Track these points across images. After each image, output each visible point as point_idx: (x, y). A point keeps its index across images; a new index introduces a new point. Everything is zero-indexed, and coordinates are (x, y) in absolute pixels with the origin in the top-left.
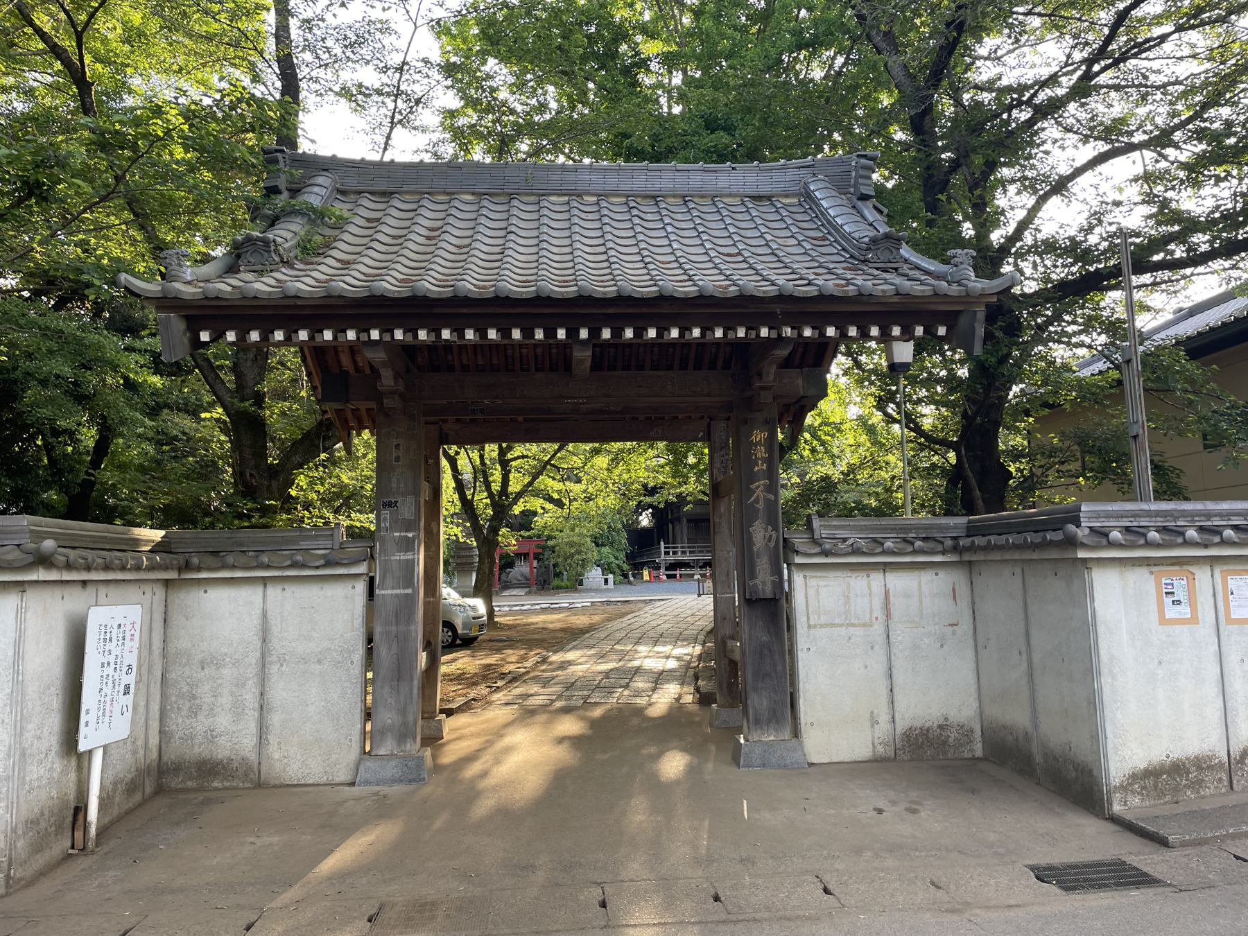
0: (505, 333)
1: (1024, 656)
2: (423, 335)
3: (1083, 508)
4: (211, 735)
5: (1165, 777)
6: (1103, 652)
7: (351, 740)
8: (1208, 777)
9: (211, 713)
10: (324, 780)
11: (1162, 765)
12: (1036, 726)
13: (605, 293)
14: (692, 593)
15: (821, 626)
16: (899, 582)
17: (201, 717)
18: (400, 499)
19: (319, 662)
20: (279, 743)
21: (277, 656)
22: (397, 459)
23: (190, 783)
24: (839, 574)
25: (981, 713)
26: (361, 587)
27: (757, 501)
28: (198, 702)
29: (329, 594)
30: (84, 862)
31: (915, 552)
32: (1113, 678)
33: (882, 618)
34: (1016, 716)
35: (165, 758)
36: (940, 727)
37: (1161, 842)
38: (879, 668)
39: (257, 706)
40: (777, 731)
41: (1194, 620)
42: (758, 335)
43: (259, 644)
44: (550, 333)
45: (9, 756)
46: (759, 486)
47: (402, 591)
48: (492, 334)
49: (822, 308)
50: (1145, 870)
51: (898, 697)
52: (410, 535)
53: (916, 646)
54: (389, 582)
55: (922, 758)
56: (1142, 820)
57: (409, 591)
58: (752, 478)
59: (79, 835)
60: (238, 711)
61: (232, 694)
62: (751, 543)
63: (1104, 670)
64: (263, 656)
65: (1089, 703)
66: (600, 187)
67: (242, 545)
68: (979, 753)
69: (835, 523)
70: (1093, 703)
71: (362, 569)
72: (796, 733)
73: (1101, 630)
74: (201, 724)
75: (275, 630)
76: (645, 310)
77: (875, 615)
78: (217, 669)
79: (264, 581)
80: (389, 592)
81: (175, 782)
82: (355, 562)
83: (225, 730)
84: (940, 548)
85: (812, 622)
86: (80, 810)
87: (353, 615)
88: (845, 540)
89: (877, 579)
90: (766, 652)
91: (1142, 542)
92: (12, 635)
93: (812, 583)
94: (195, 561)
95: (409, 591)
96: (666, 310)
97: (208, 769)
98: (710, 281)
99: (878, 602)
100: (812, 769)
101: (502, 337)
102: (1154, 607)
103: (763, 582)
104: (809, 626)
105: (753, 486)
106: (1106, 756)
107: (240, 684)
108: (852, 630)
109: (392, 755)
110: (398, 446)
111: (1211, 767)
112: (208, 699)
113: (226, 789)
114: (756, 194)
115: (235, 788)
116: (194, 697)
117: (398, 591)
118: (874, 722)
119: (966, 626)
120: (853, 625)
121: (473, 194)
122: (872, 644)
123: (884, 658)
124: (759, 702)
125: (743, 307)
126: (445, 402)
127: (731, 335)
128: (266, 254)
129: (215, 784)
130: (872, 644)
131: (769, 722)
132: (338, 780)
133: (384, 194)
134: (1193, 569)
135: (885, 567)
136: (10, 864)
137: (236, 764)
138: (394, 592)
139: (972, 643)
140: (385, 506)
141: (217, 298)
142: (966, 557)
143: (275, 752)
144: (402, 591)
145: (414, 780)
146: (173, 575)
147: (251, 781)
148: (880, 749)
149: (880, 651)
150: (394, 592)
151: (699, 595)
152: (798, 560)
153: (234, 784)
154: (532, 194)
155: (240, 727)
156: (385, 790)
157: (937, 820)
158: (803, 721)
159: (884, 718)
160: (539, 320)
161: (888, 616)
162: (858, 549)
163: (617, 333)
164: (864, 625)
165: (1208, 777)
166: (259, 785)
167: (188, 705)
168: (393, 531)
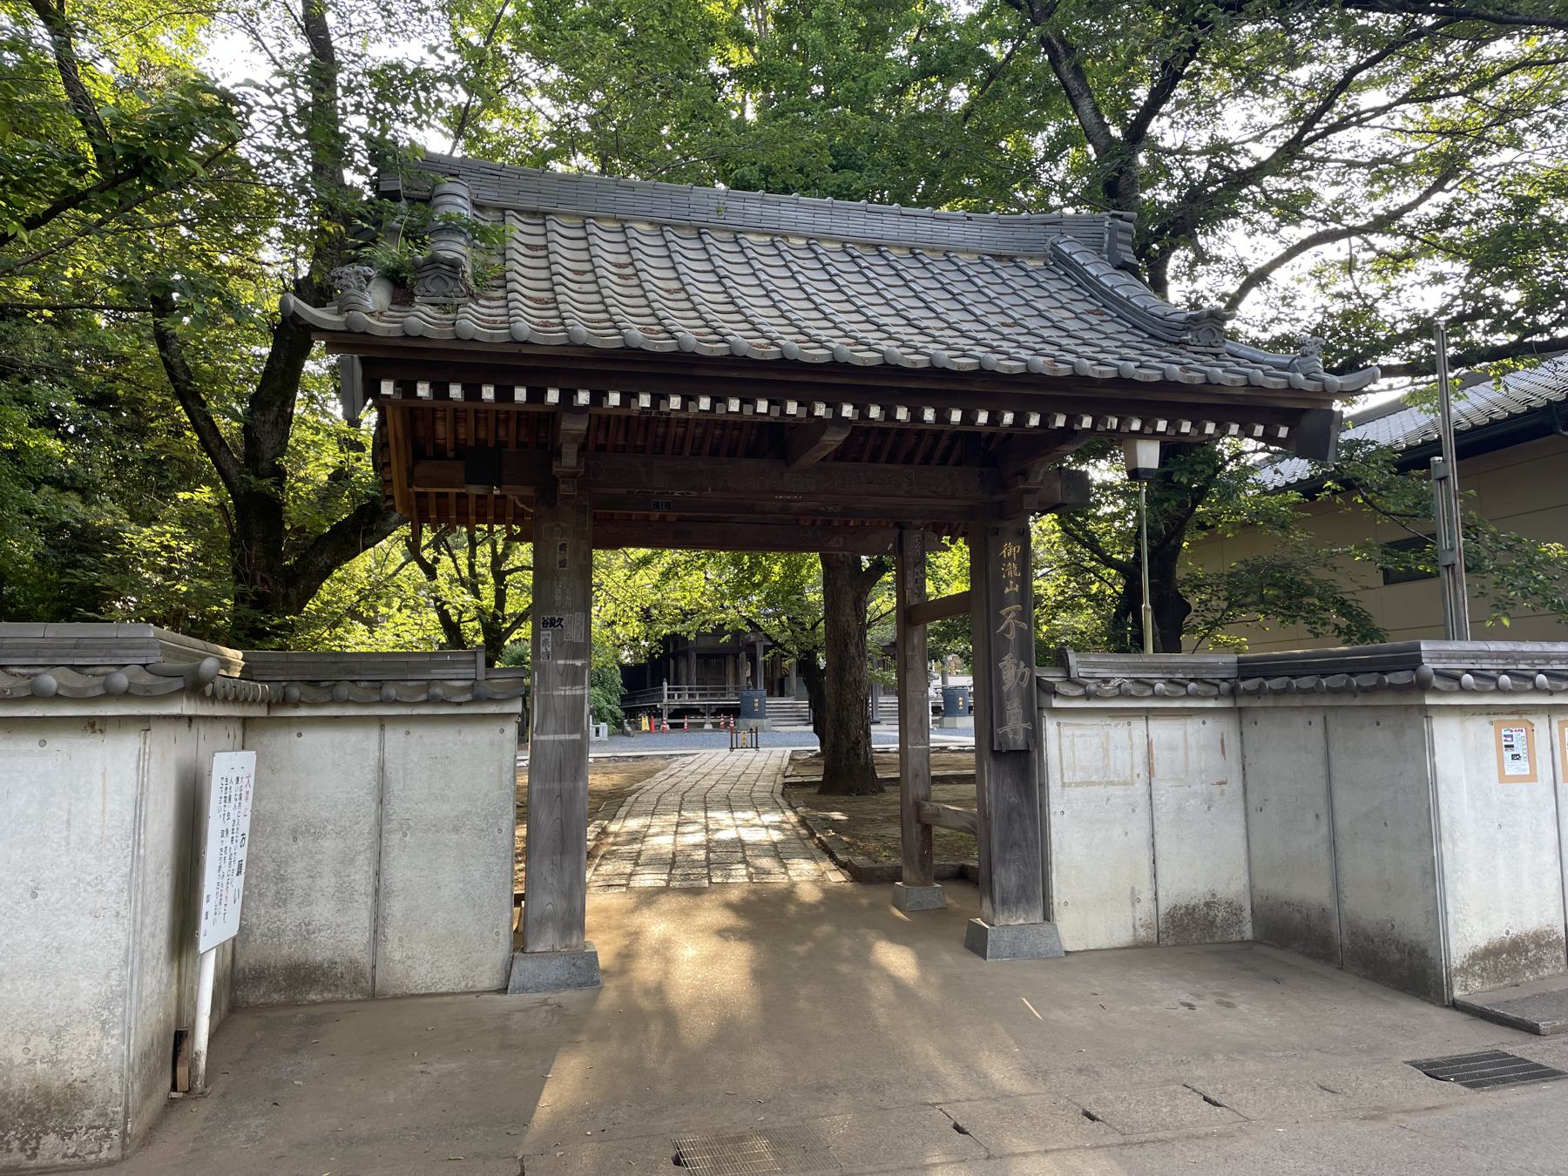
0: (862, 409)
1: (1324, 819)
2: (762, 406)
3: (1423, 647)
4: (306, 931)
5: (1506, 955)
6: (1443, 814)
7: (498, 934)
8: (1547, 955)
9: (307, 900)
10: (462, 987)
11: (1502, 943)
12: (1339, 902)
13: (712, 350)
14: (723, 746)
15: (1078, 784)
16: (1164, 732)
17: (293, 906)
18: (566, 617)
19: (456, 830)
20: (401, 939)
21: (382, 827)
22: (563, 563)
23: (275, 996)
24: (1096, 721)
25: (1252, 887)
26: (511, 730)
27: (1007, 630)
28: (288, 885)
29: (470, 739)
30: (199, 1112)
31: (1188, 696)
32: (1454, 843)
33: (1144, 775)
34: (1311, 890)
35: (241, 963)
36: (1207, 904)
37: (1532, 1030)
38: (1140, 836)
39: (370, 889)
40: (1026, 912)
41: (1532, 777)
42: (783, 412)
43: (374, 805)
44: (536, 395)
45: (126, 962)
46: (1010, 612)
47: (568, 737)
48: (875, 412)
49: (1074, 391)
50: (1536, 1060)
51: (1161, 871)
52: (579, 663)
53: (1181, 809)
54: (551, 723)
55: (1188, 939)
56: (1498, 1005)
57: (577, 737)
58: (1003, 601)
59: (182, 1071)
60: (344, 895)
61: (337, 874)
62: (1000, 682)
63: (1445, 835)
64: (379, 823)
65: (1425, 873)
66: (809, 228)
67: (352, 672)
68: (1248, 933)
69: (1093, 659)
70: (1431, 873)
71: (517, 707)
72: (1048, 916)
73: (1442, 788)
74: (292, 916)
75: (396, 788)
76: (952, 387)
77: (1136, 771)
78: (316, 840)
79: (382, 721)
80: (551, 737)
81: (255, 996)
82: (509, 699)
83: (331, 926)
84: (1215, 691)
85: (1066, 780)
86: (181, 1037)
87: (501, 768)
88: (1106, 681)
89: (1139, 726)
90: (1014, 816)
91: (1493, 687)
92: (130, 791)
93: (1067, 731)
94: (295, 692)
95: (577, 737)
96: (976, 388)
97: (302, 976)
98: (956, 353)
99: (1139, 756)
100: (1069, 959)
101: (435, 397)
102: (1494, 762)
103: (1014, 729)
104: (1063, 785)
105: (1003, 612)
106: (1446, 934)
107: (348, 860)
108: (1111, 789)
109: (553, 953)
110: (563, 547)
111: (1549, 944)
112: (302, 881)
113: (326, 1002)
114: (997, 252)
115: (339, 1001)
116: (283, 879)
117: (562, 737)
118: (1135, 900)
119: (1235, 785)
120: (1112, 783)
121: (651, 223)
122: (1135, 801)
123: (1146, 824)
124: (1006, 878)
125: (981, 385)
126: (624, 491)
127: (720, 409)
128: (451, 283)
129: (312, 997)
130: (1135, 801)
131: (1018, 901)
132: (480, 986)
133: (533, 213)
134: (1532, 719)
135: (1148, 713)
136: (126, 1117)
137: (341, 969)
138: (557, 737)
139: (1242, 804)
140: (545, 624)
141: (421, 337)
142: (1243, 703)
143: (394, 951)
144: (568, 737)
145: (585, 984)
146: (260, 712)
147: (362, 991)
148: (1142, 933)
149: (1142, 814)
150: (557, 737)
151: (732, 749)
152: (1056, 703)
153: (339, 996)
154: (726, 230)
155: (347, 918)
156: (554, 997)
157: (1254, 1016)
158: (1055, 900)
159: (1146, 895)
160: (928, 397)
161: (1151, 772)
162: (1127, 691)
163: (504, 394)
164: (1125, 783)
165: (1547, 955)
166: (373, 996)
167: (273, 888)
168: (555, 657)
